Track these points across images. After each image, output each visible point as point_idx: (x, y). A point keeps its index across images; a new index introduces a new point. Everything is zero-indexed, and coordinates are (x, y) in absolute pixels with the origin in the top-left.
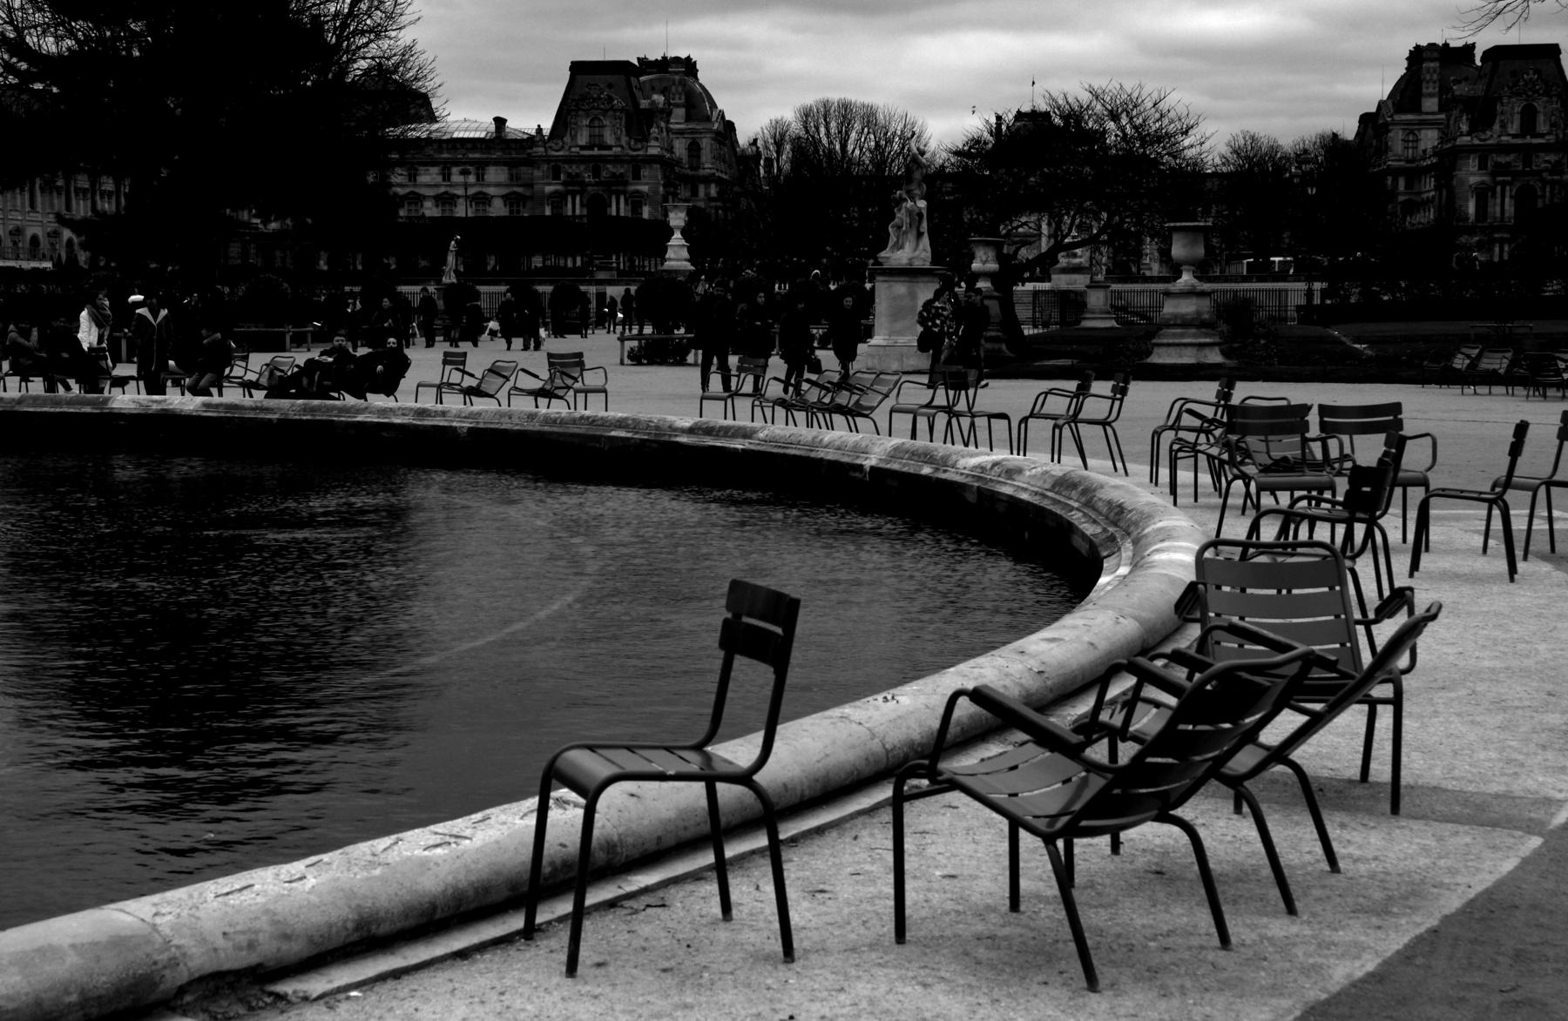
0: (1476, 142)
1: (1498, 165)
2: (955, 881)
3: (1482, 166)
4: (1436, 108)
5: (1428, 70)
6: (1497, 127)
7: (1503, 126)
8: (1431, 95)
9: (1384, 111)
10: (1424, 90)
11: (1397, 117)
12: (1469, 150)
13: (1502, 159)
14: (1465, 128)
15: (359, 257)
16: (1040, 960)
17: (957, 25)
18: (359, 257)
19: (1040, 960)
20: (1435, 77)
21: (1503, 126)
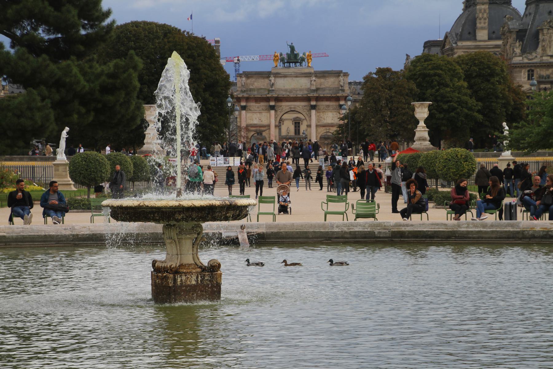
0: (526, 61)
1: (540, 77)
2: (345, 267)
3: (530, 77)
4: (486, 38)
5: (480, 10)
6: (539, 50)
7: (544, 50)
8: (482, 28)
9: (450, 38)
10: (478, 25)
11: (460, 44)
12: (522, 66)
13: (544, 72)
14: (518, 51)
15: (67, 129)
16: (277, 124)
17: (530, 156)
18: (67, 129)
19: (277, 124)
20: (485, 15)
21: (544, 50)
